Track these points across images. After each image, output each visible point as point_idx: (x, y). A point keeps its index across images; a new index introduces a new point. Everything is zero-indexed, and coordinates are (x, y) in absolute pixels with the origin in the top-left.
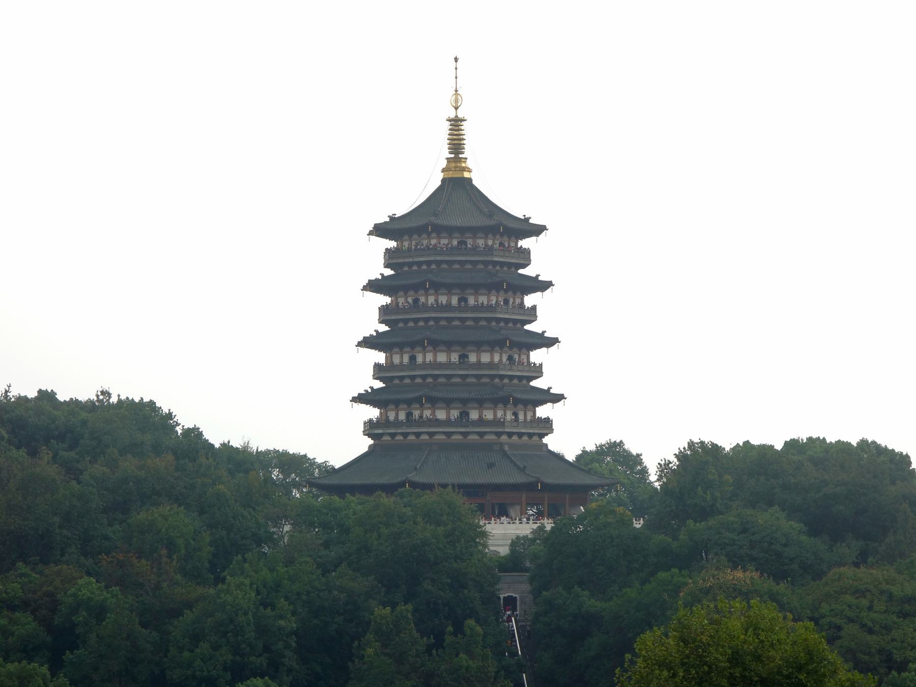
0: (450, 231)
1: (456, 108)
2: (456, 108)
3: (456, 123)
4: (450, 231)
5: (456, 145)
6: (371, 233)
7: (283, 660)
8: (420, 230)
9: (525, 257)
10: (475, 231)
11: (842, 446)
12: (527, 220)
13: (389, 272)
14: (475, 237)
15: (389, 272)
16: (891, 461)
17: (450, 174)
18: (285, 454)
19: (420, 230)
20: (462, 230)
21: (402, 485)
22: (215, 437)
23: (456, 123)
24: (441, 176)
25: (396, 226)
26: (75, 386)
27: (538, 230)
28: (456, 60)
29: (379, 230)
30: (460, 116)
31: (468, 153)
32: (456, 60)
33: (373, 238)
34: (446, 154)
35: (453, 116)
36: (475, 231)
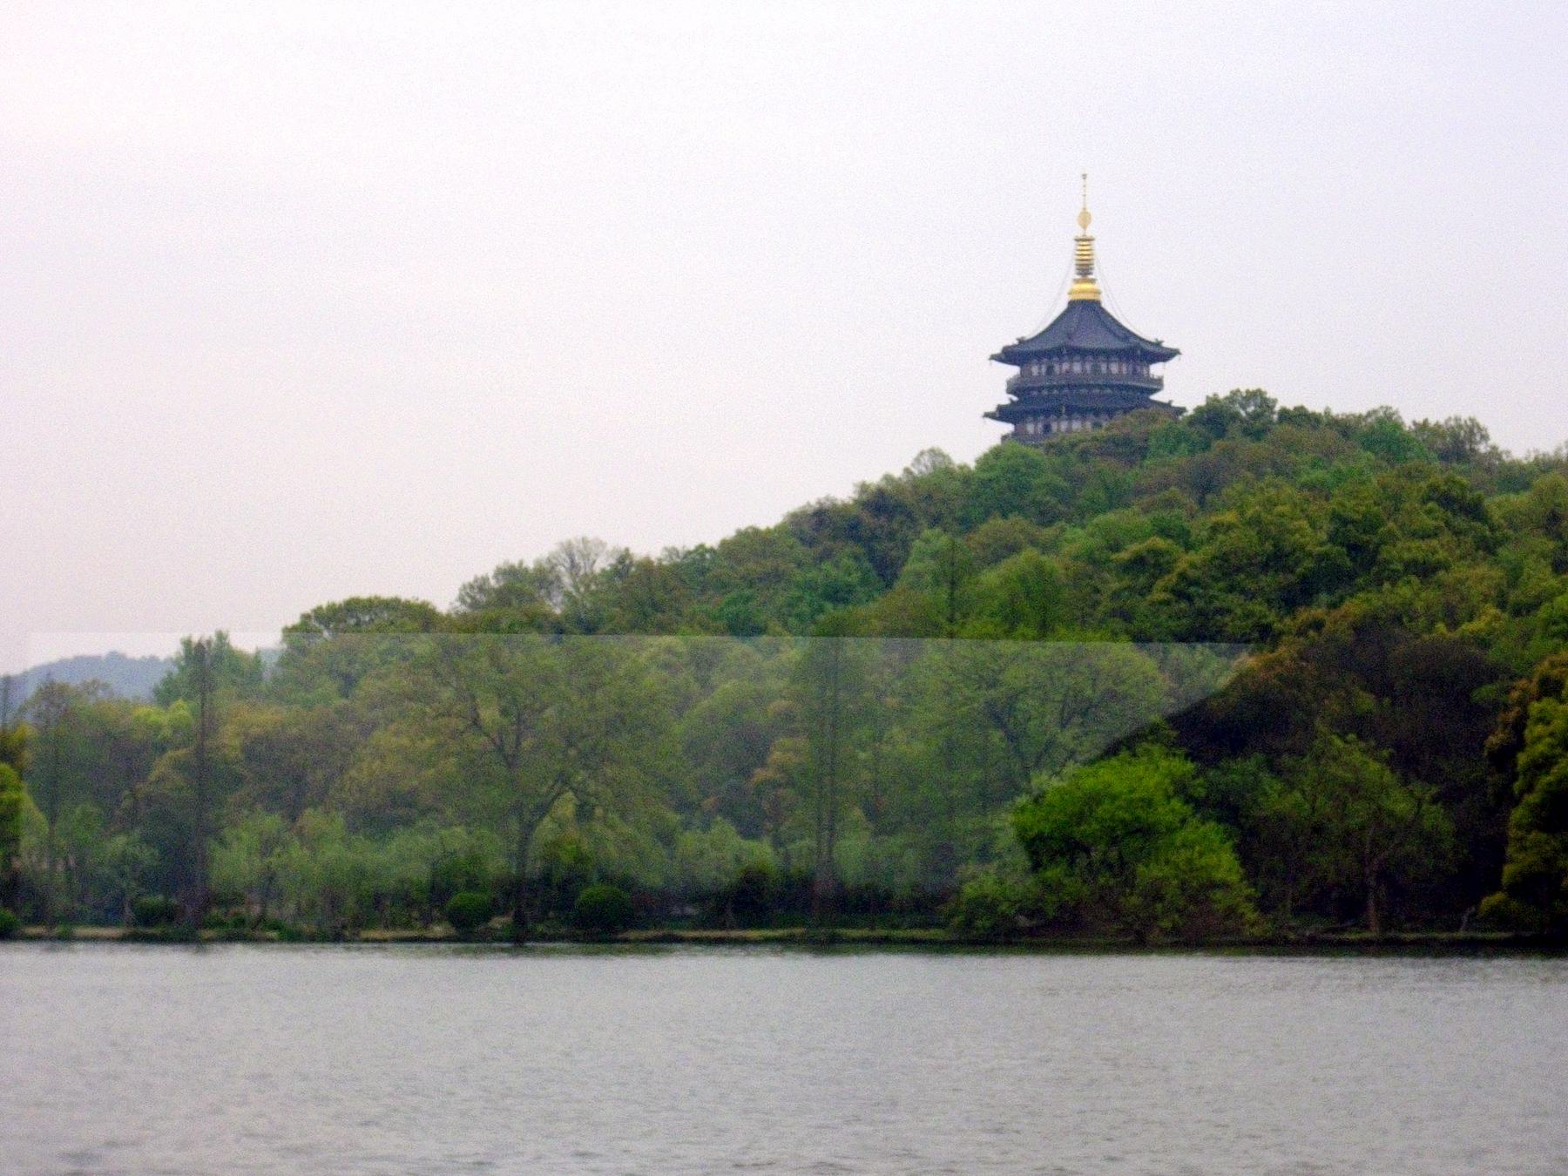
0: (1082, 353)
1: (1084, 228)
2: (1084, 228)
4: (1082, 353)
5: (1085, 270)
7: (1435, 790)
8: (1059, 353)
10: (1108, 354)
11: (749, 545)
12: (1158, 344)
14: (1108, 362)
18: (397, 601)
19: (1059, 353)
20: (1095, 353)
21: (511, 629)
27: (1166, 355)
28: (1084, 176)
29: (1008, 356)
30: (1089, 235)
32: (1084, 176)
33: (1168, 344)
35: (1080, 236)
36: (1108, 354)
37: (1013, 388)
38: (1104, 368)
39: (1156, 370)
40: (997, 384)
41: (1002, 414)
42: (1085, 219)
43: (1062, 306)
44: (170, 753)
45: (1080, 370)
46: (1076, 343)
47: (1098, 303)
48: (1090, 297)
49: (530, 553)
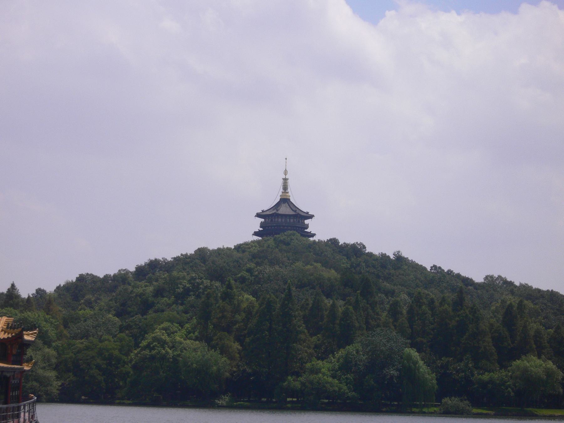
3: (285, 180)
5: (285, 188)
6: (13, 285)
9: (307, 227)
12: (308, 213)
13: (261, 229)
14: (290, 219)
15: (261, 229)
16: (459, 303)
17: (283, 197)
22: (374, 248)
23: (285, 180)
24: (280, 198)
25: (264, 213)
26: (241, 242)
27: (311, 217)
29: (258, 215)
31: (289, 190)
33: (9, 286)
34: (282, 190)
35: (284, 178)
36: (290, 216)
37: (262, 225)
38: (288, 220)
39: (306, 222)
40: (256, 224)
41: (256, 234)
42: (286, 172)
43: (278, 200)
44: (277, 267)
45: (283, 222)
46: (279, 212)
47: (289, 199)
48: (285, 197)
49: (160, 258)
